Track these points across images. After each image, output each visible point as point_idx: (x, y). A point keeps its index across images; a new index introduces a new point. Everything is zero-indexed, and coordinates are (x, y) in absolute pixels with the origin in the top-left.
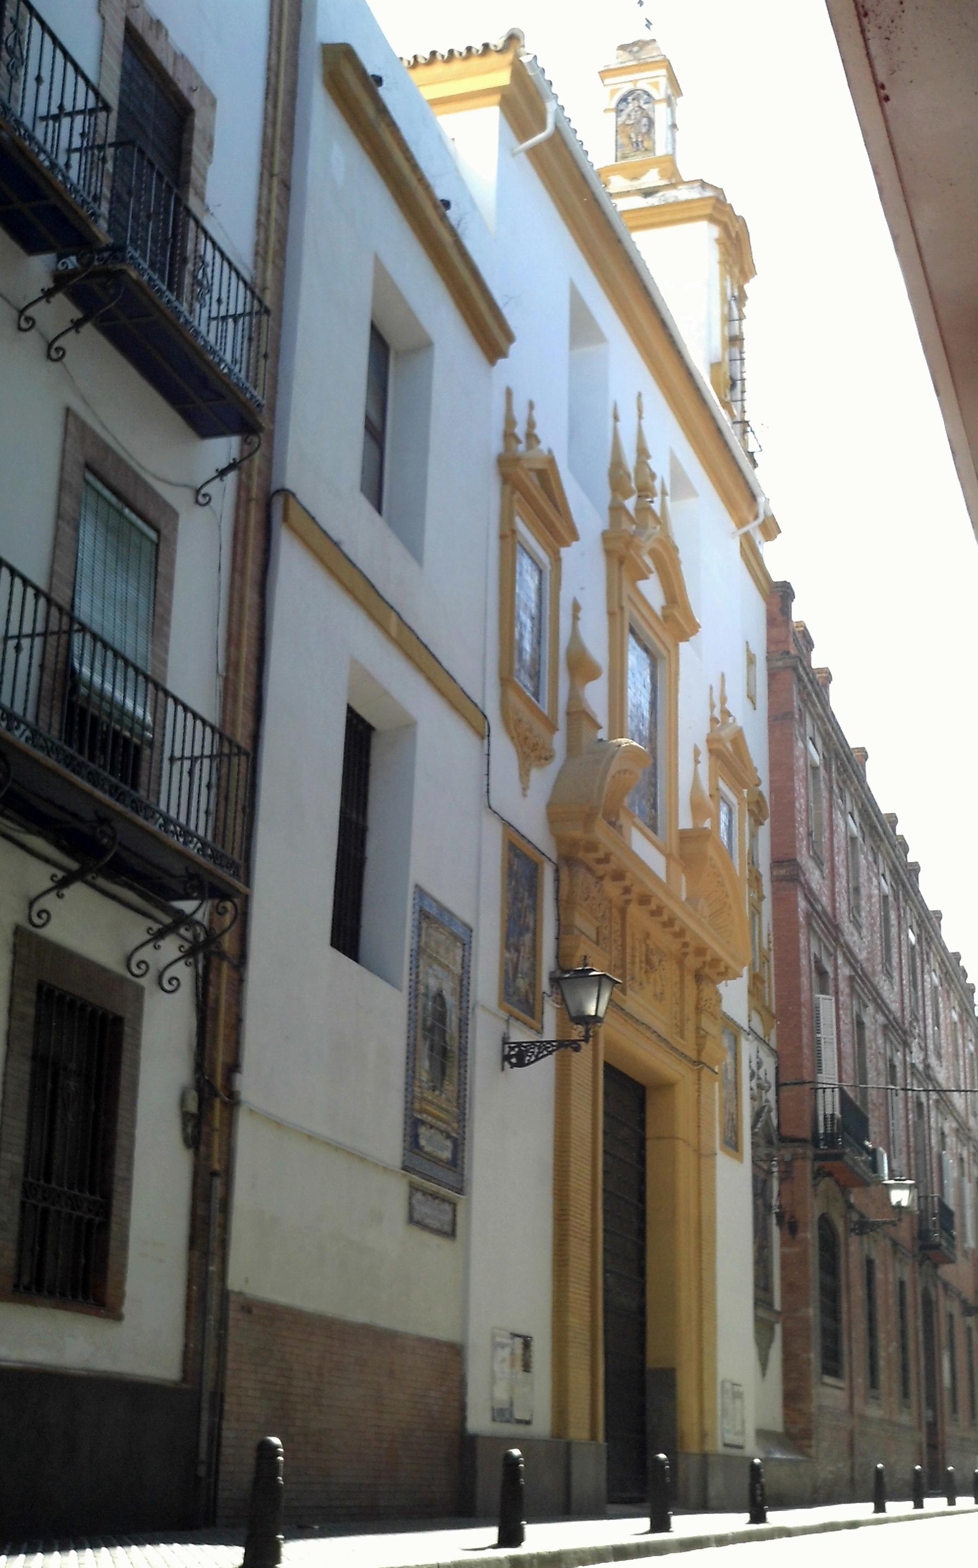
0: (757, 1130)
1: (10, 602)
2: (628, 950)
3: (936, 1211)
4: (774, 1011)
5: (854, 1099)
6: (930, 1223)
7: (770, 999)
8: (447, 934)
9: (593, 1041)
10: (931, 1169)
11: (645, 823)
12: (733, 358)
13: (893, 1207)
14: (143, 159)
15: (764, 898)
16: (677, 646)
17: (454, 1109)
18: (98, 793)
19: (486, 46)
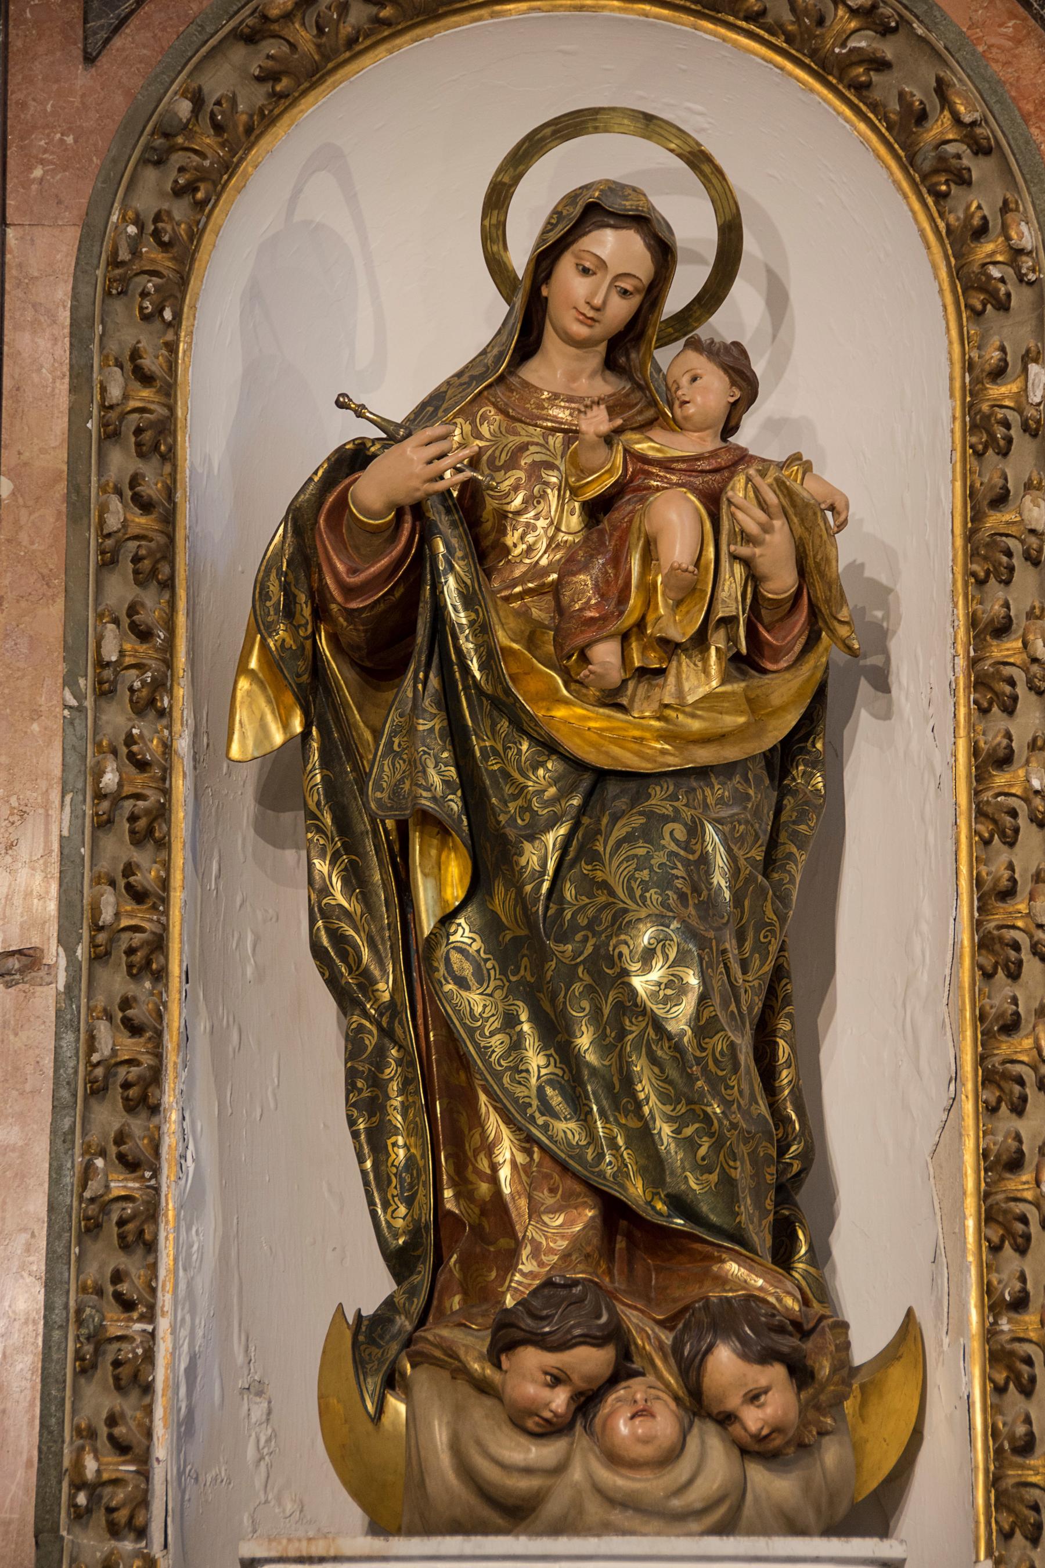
0: (997, 1554)
1: (817, 1560)
2: (704, 756)
3: (155, 917)
4: (688, 1404)
5: (508, 1199)
6: (393, 1139)
7: (425, 890)
8: (501, 1009)
9: (194, 1347)
10: (181, 955)
11: (72, 1552)
12: (823, 1430)
13: (507, 1310)
14: (192, 1278)
15: (168, 140)
16: (859, 1368)
17: (789, 1301)
18: (94, 479)
19: (1026, 1447)
